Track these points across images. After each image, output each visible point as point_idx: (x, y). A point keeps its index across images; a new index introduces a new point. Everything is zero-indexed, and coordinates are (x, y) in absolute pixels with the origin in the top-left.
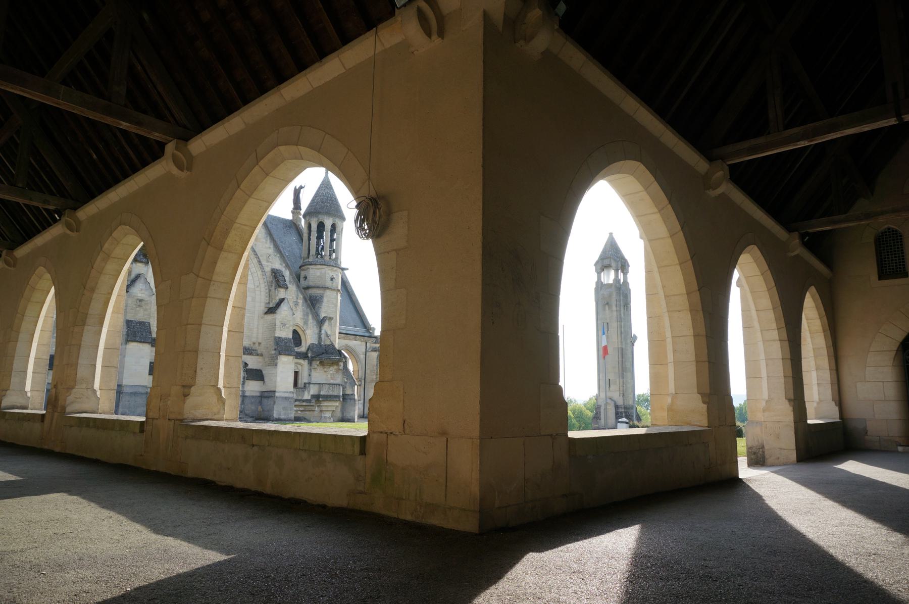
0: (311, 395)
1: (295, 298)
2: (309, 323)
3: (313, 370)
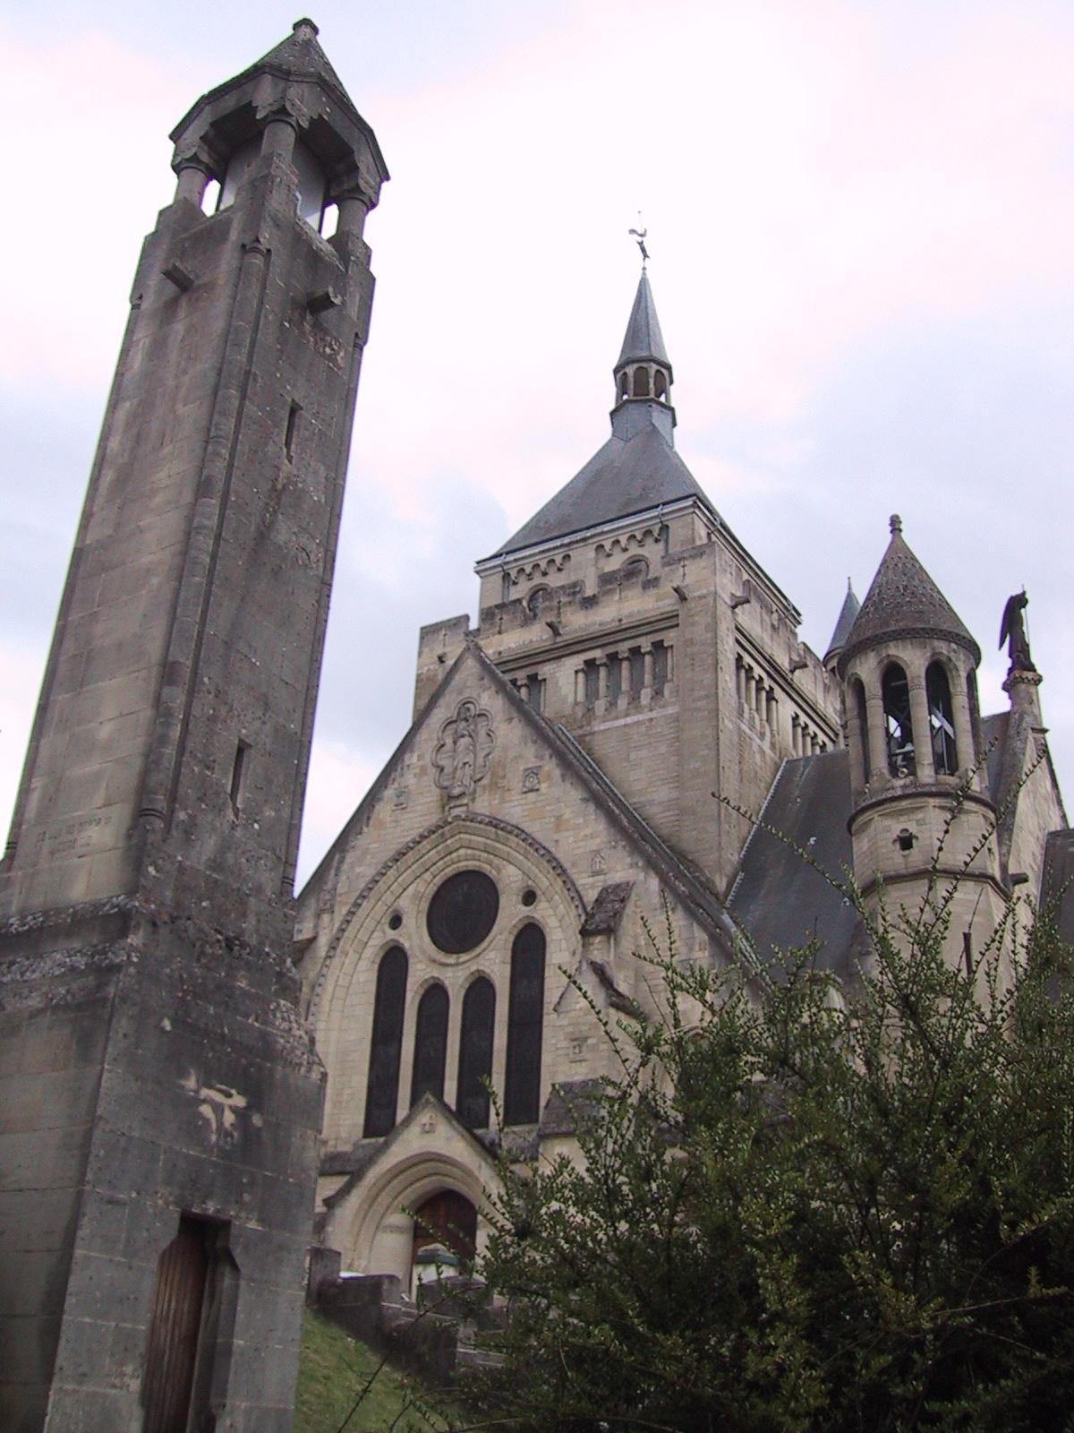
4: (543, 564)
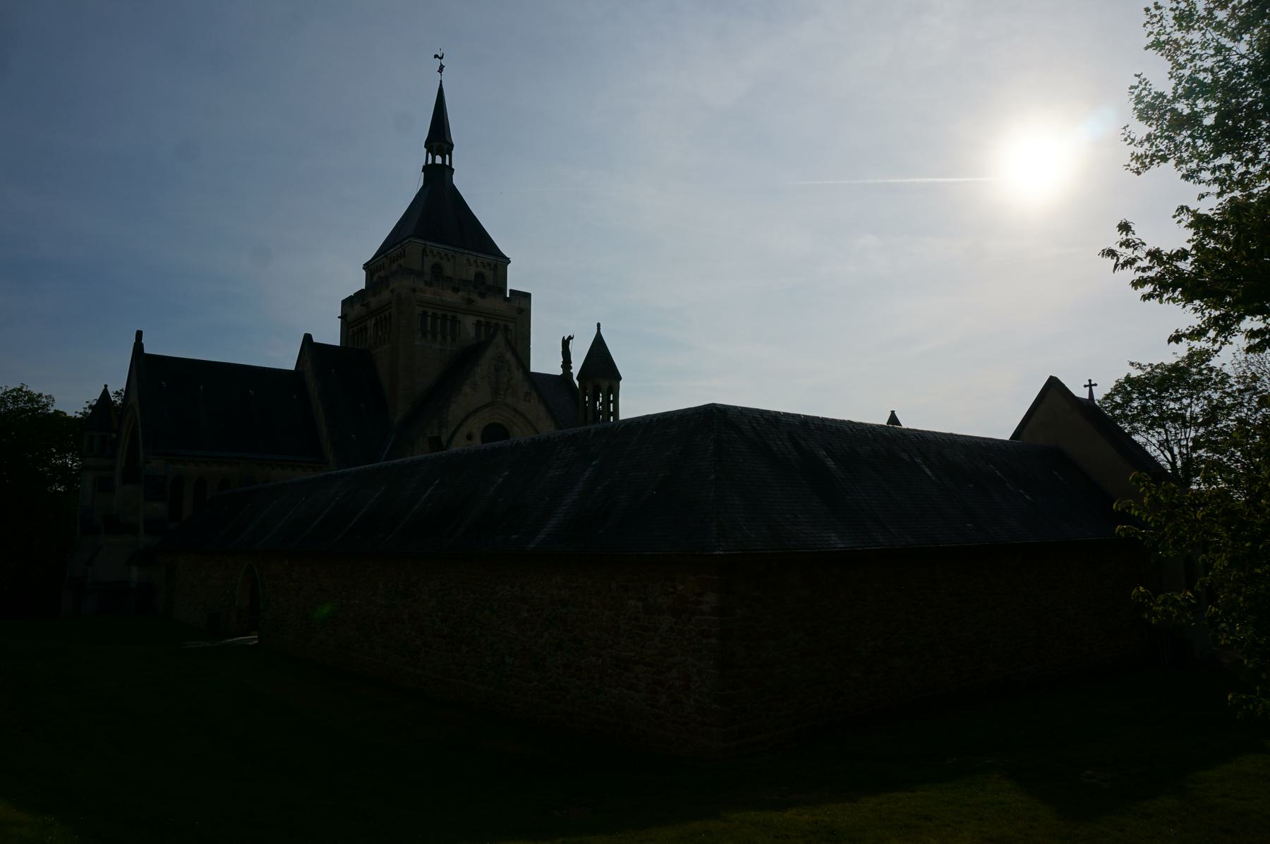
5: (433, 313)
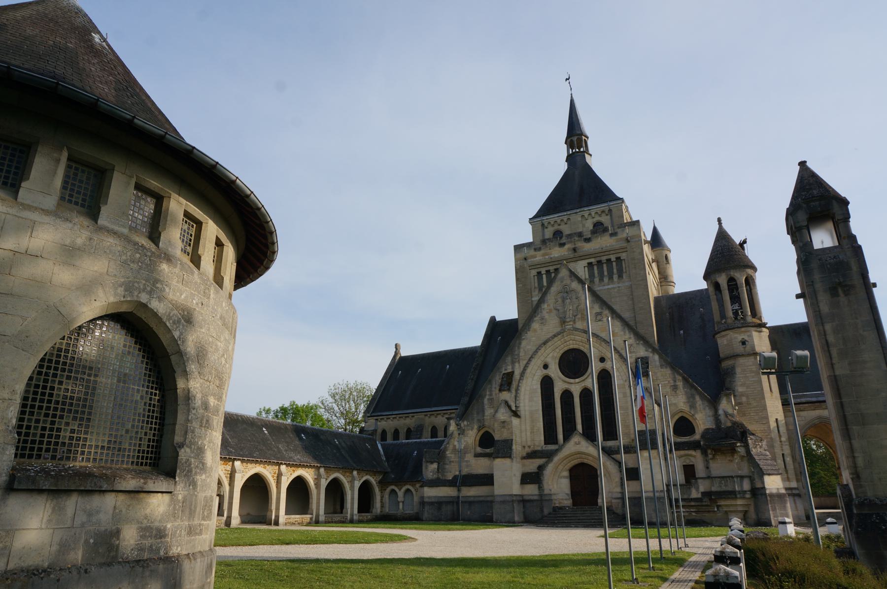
0: (702, 493)
1: (672, 382)
2: (697, 405)
3: (711, 461)
4: (559, 221)
5: (547, 271)
